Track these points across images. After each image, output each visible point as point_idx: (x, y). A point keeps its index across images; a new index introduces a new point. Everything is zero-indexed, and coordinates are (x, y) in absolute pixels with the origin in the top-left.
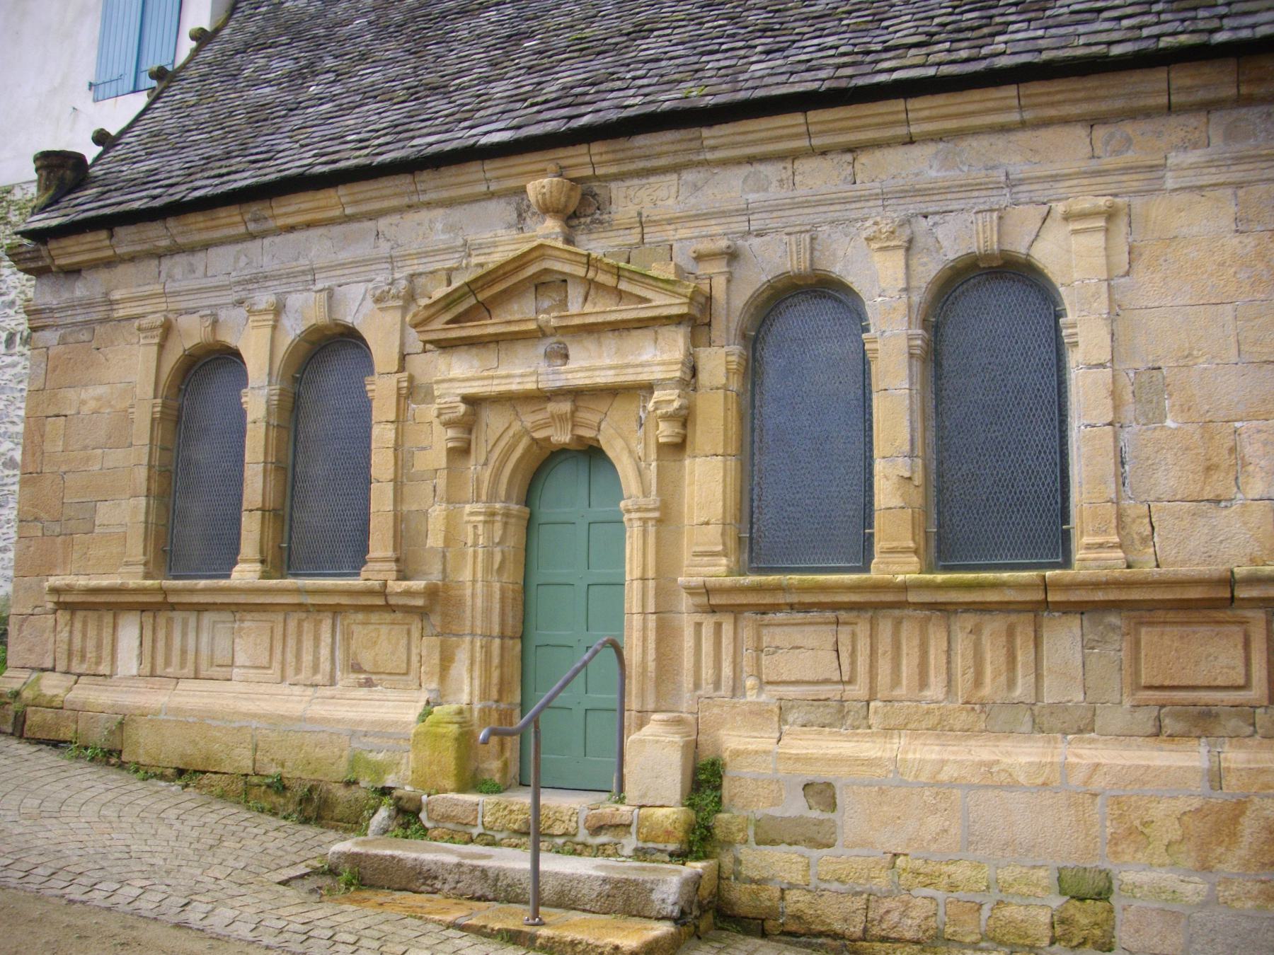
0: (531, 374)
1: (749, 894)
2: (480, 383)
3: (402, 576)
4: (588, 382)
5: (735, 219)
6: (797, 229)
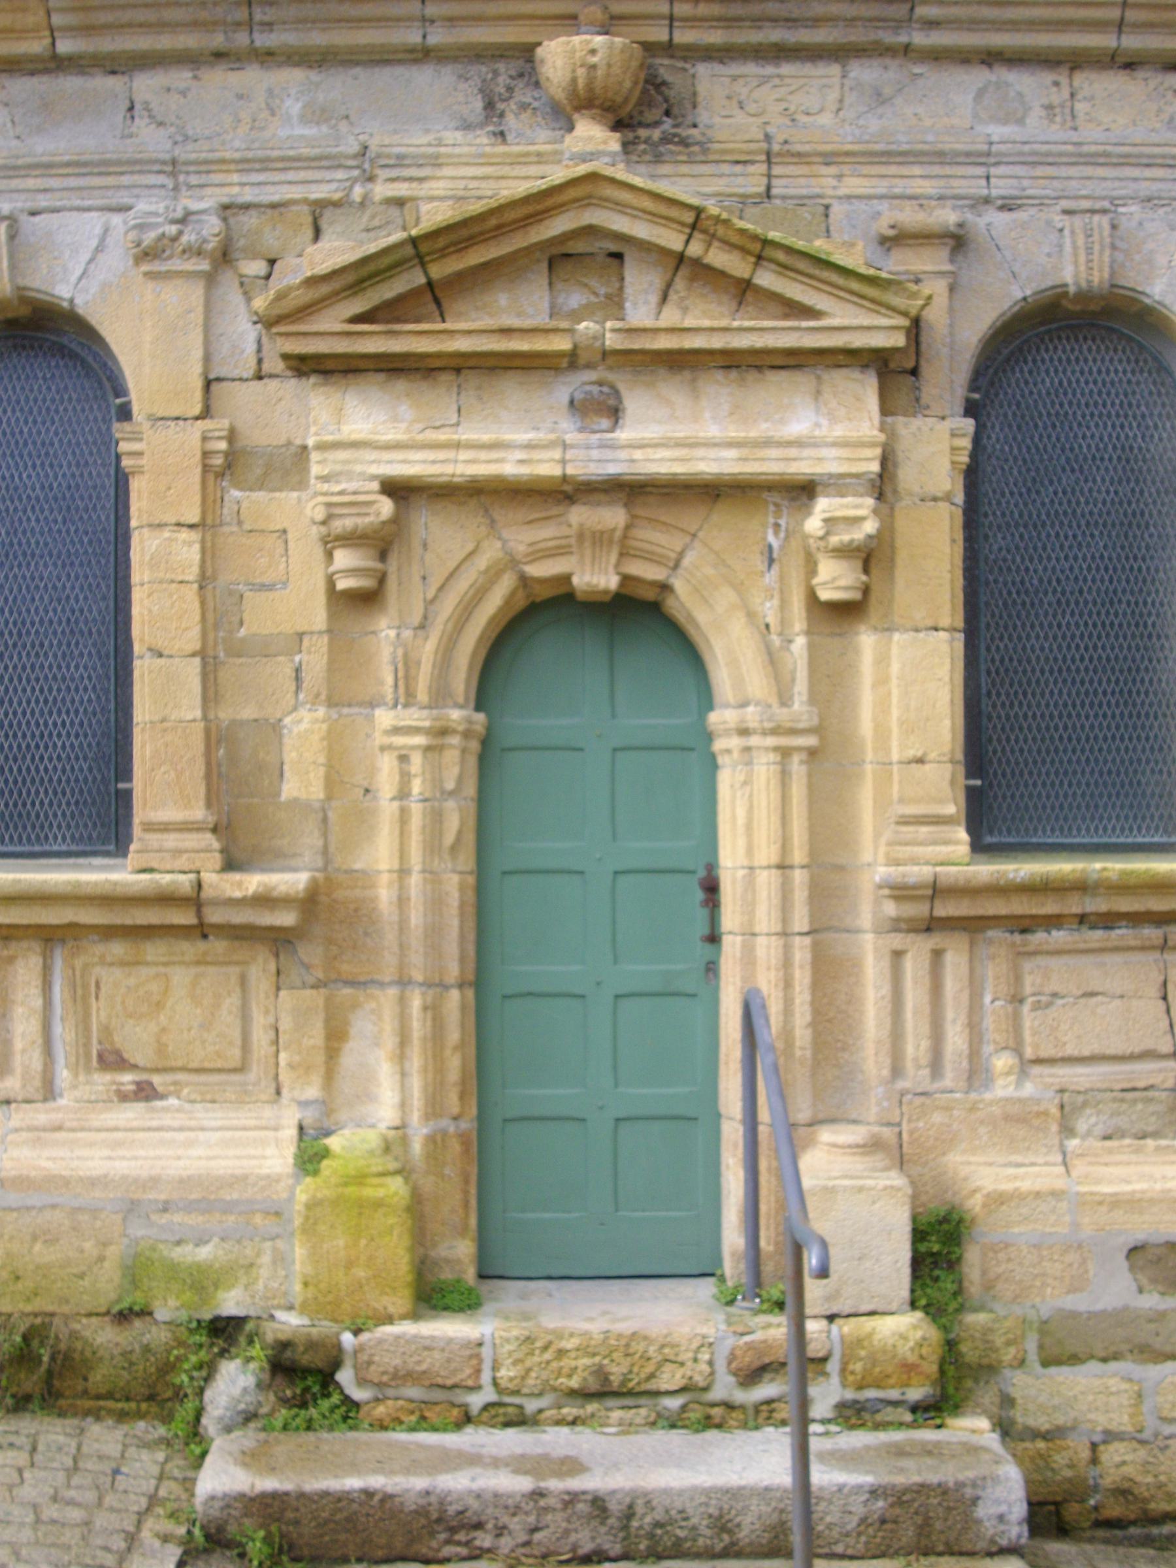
0: (550, 445)
1: (1032, 1459)
3: (230, 865)
4: (679, 469)
6: (1086, 204)
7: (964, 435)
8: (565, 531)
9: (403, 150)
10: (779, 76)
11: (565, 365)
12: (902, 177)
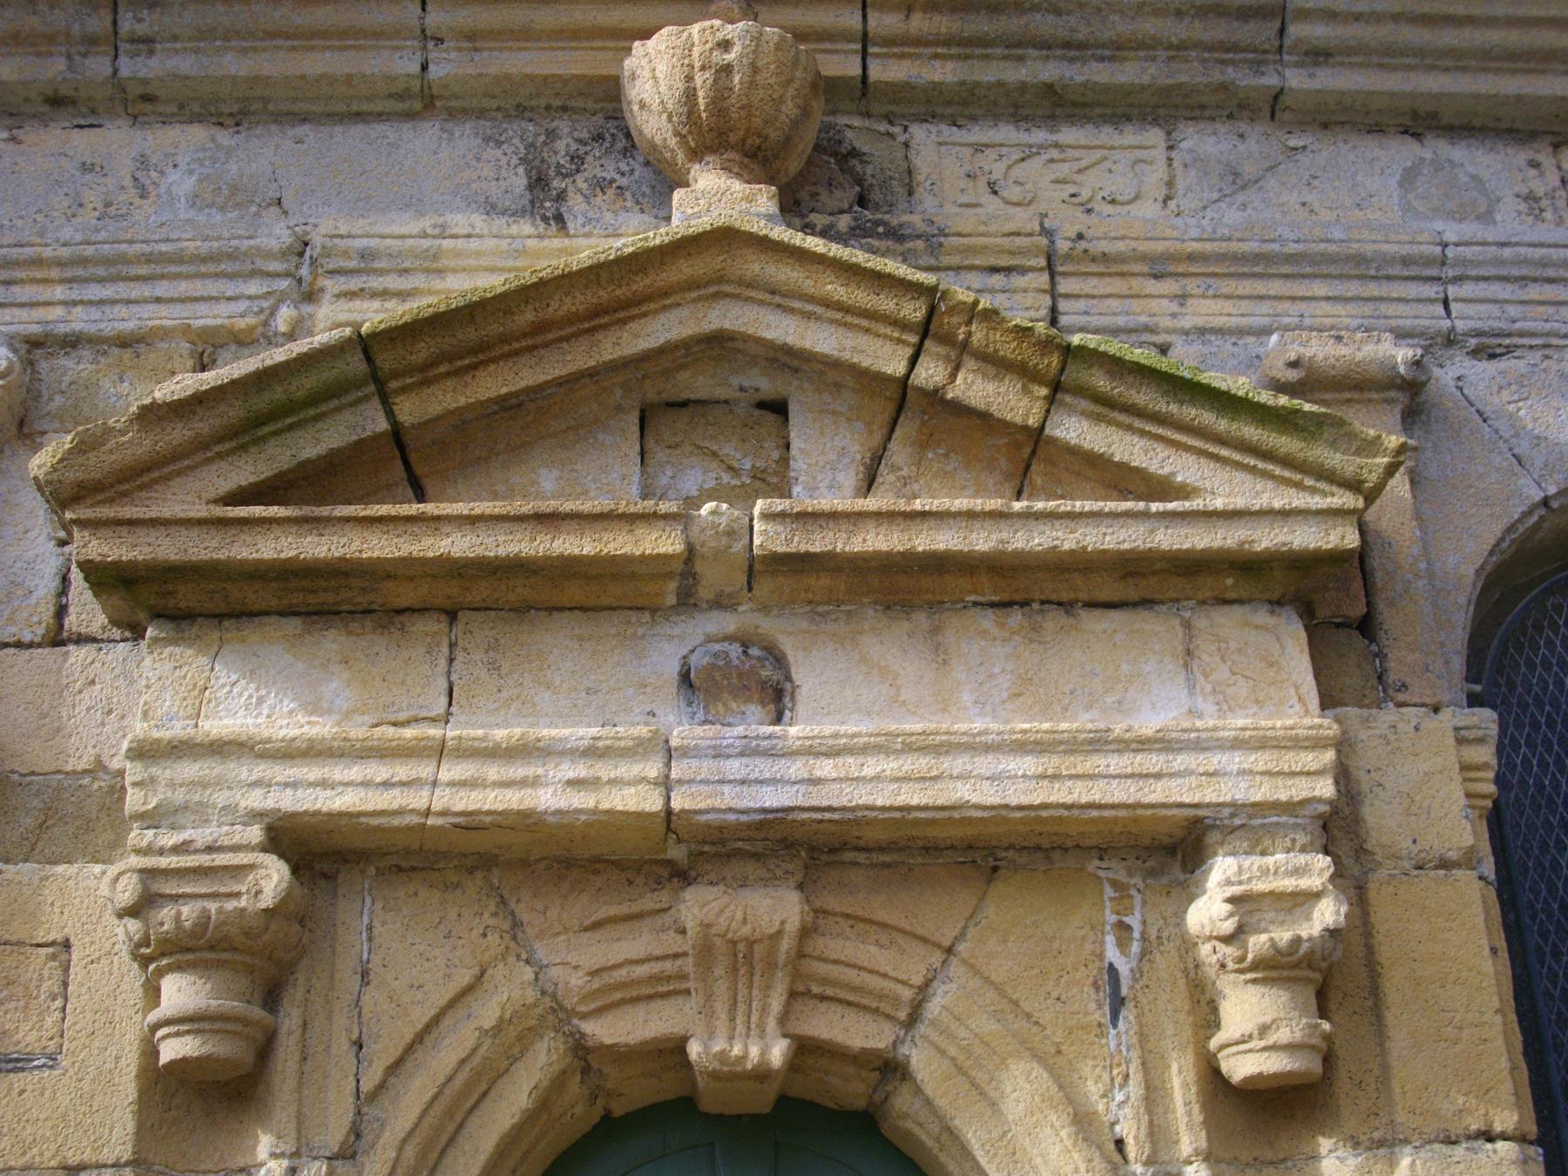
0: (637, 750)
2: (380, 771)
4: (912, 796)
5: (1397, 289)
7: (1480, 741)
8: (672, 942)
9: (373, 243)
10: (1056, 145)
11: (671, 600)
12: (1293, 299)
